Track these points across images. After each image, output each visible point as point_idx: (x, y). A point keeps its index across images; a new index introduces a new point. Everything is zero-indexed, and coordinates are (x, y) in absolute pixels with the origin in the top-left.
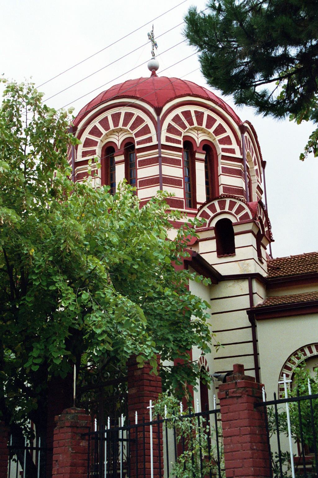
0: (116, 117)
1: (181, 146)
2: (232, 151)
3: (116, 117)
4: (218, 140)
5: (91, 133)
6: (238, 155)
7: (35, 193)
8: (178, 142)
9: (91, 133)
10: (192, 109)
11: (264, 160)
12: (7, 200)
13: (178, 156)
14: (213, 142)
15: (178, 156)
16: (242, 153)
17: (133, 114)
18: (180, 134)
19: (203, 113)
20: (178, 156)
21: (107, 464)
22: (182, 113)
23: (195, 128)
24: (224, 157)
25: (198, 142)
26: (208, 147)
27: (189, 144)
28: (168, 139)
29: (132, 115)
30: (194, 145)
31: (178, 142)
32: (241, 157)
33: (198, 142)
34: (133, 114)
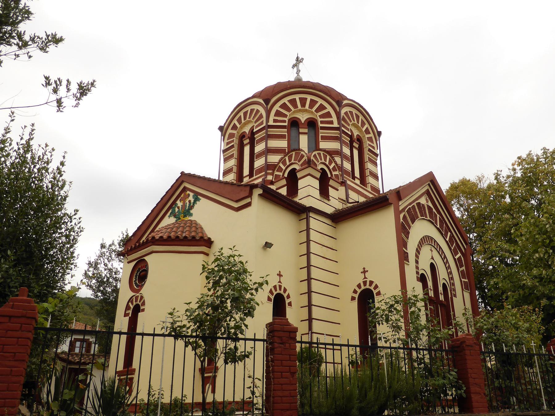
0: (313, 103)
1: (286, 124)
2: (331, 123)
3: (313, 103)
4: (319, 116)
5: (290, 101)
6: (336, 125)
7: (43, 247)
8: (285, 121)
9: (290, 101)
10: (285, 100)
11: (379, 130)
12: (56, 227)
13: (284, 132)
14: (316, 118)
15: (284, 132)
16: (339, 123)
17: (325, 108)
18: (285, 116)
19: (285, 103)
20: (284, 132)
21: (254, 184)
22: (288, 101)
23: (300, 110)
24: (323, 128)
25: (303, 120)
26: (359, 140)
27: (294, 123)
28: (275, 121)
29: (325, 108)
30: (299, 123)
31: (285, 121)
32: (338, 126)
33: (303, 120)
34: (325, 108)
